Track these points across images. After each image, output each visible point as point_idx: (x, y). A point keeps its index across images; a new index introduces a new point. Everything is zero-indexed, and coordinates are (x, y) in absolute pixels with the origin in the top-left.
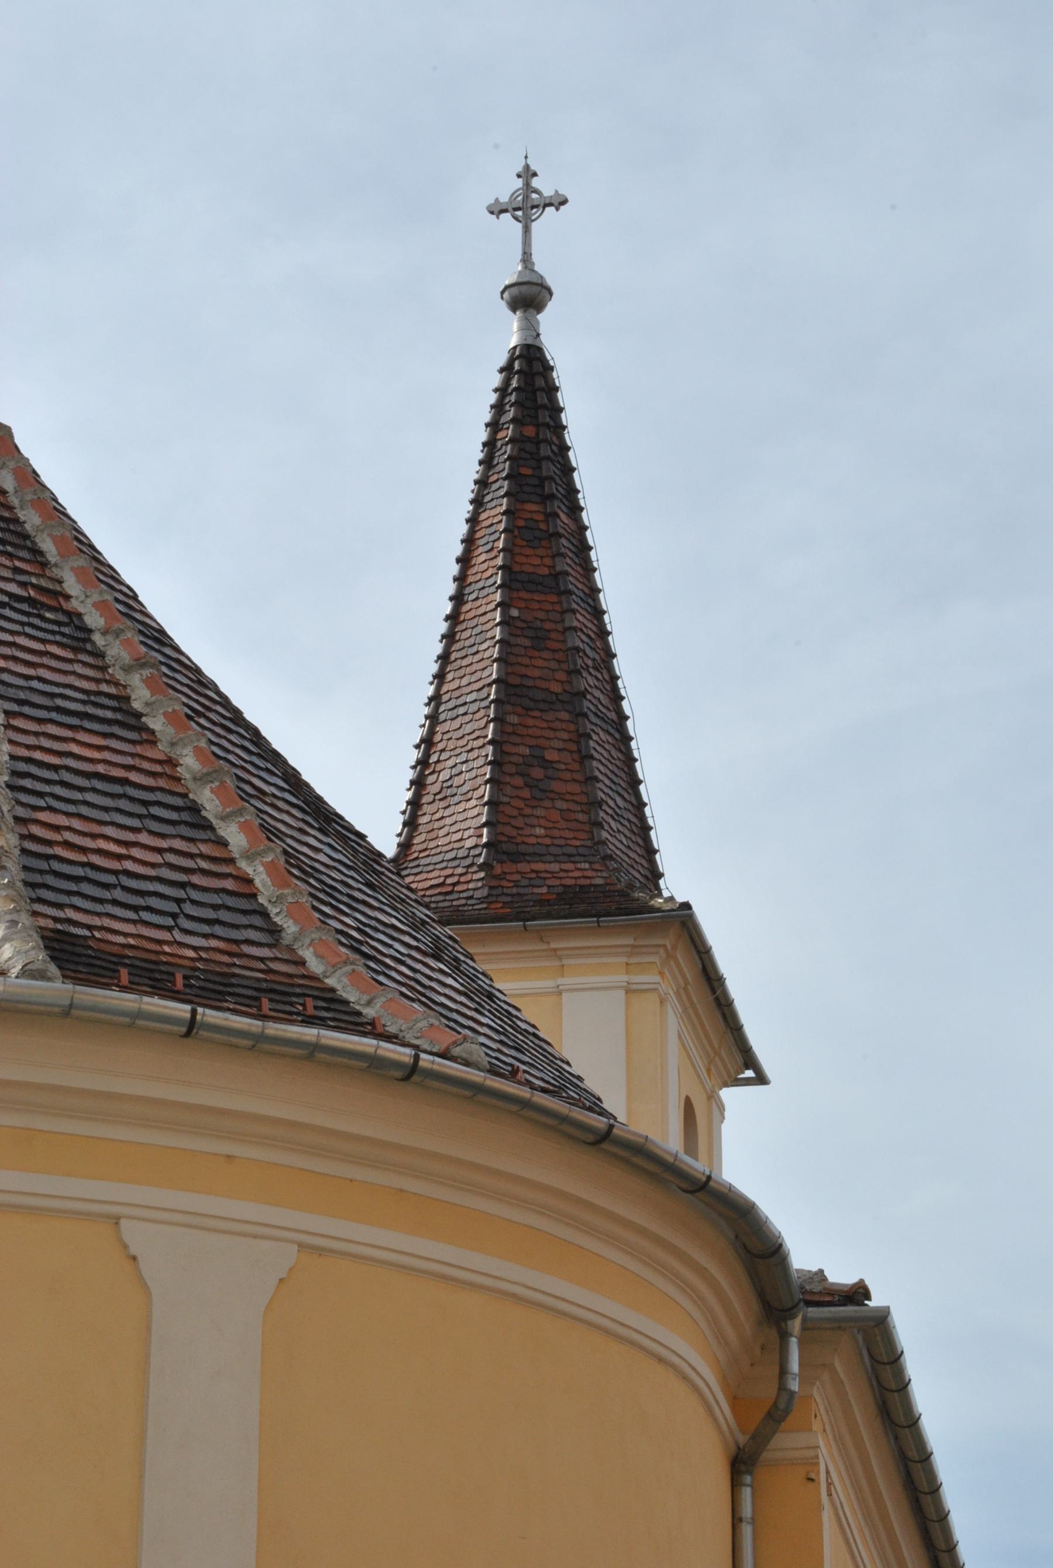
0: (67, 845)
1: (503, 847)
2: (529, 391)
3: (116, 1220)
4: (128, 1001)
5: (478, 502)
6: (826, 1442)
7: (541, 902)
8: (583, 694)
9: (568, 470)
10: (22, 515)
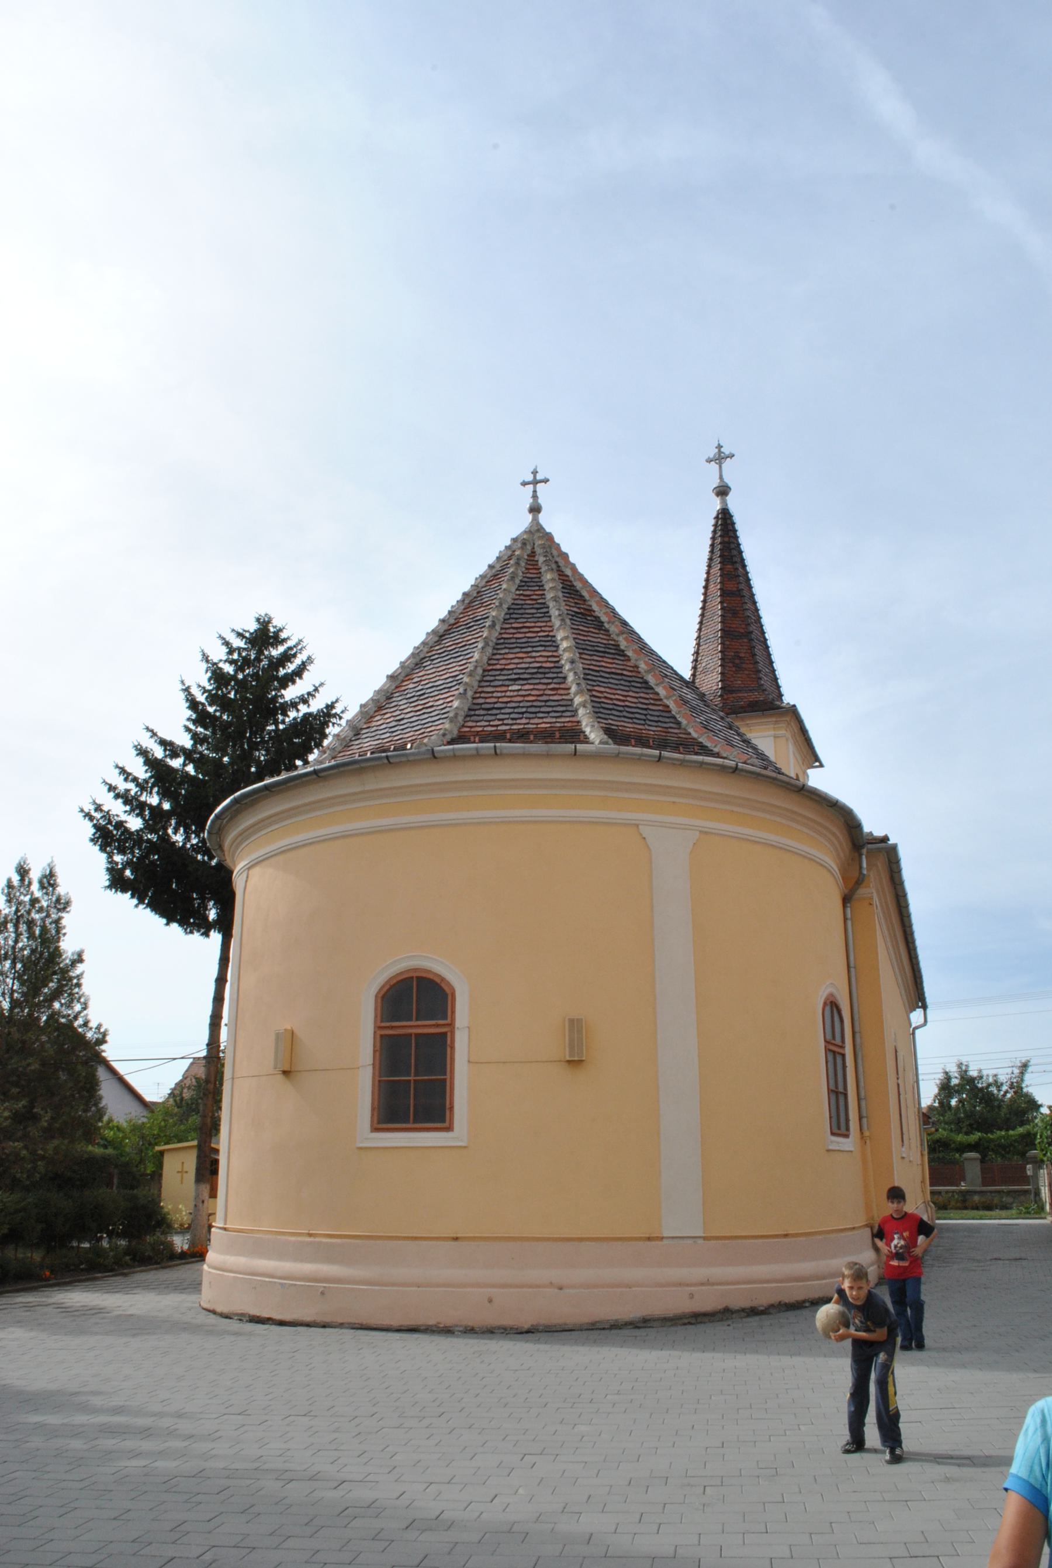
0: (606, 698)
1: (727, 688)
2: (725, 529)
3: (637, 826)
4: (638, 750)
5: (709, 566)
6: (874, 891)
7: (742, 707)
8: (752, 632)
9: (741, 552)
10: (575, 584)
